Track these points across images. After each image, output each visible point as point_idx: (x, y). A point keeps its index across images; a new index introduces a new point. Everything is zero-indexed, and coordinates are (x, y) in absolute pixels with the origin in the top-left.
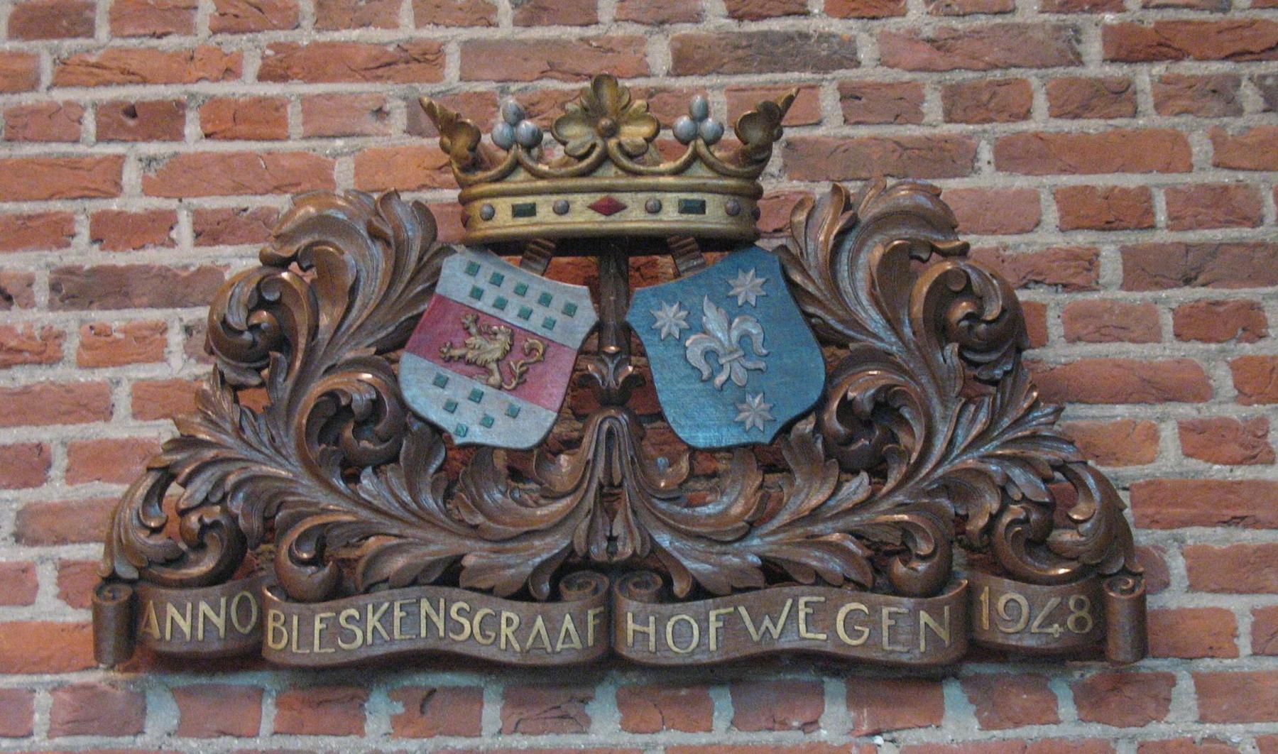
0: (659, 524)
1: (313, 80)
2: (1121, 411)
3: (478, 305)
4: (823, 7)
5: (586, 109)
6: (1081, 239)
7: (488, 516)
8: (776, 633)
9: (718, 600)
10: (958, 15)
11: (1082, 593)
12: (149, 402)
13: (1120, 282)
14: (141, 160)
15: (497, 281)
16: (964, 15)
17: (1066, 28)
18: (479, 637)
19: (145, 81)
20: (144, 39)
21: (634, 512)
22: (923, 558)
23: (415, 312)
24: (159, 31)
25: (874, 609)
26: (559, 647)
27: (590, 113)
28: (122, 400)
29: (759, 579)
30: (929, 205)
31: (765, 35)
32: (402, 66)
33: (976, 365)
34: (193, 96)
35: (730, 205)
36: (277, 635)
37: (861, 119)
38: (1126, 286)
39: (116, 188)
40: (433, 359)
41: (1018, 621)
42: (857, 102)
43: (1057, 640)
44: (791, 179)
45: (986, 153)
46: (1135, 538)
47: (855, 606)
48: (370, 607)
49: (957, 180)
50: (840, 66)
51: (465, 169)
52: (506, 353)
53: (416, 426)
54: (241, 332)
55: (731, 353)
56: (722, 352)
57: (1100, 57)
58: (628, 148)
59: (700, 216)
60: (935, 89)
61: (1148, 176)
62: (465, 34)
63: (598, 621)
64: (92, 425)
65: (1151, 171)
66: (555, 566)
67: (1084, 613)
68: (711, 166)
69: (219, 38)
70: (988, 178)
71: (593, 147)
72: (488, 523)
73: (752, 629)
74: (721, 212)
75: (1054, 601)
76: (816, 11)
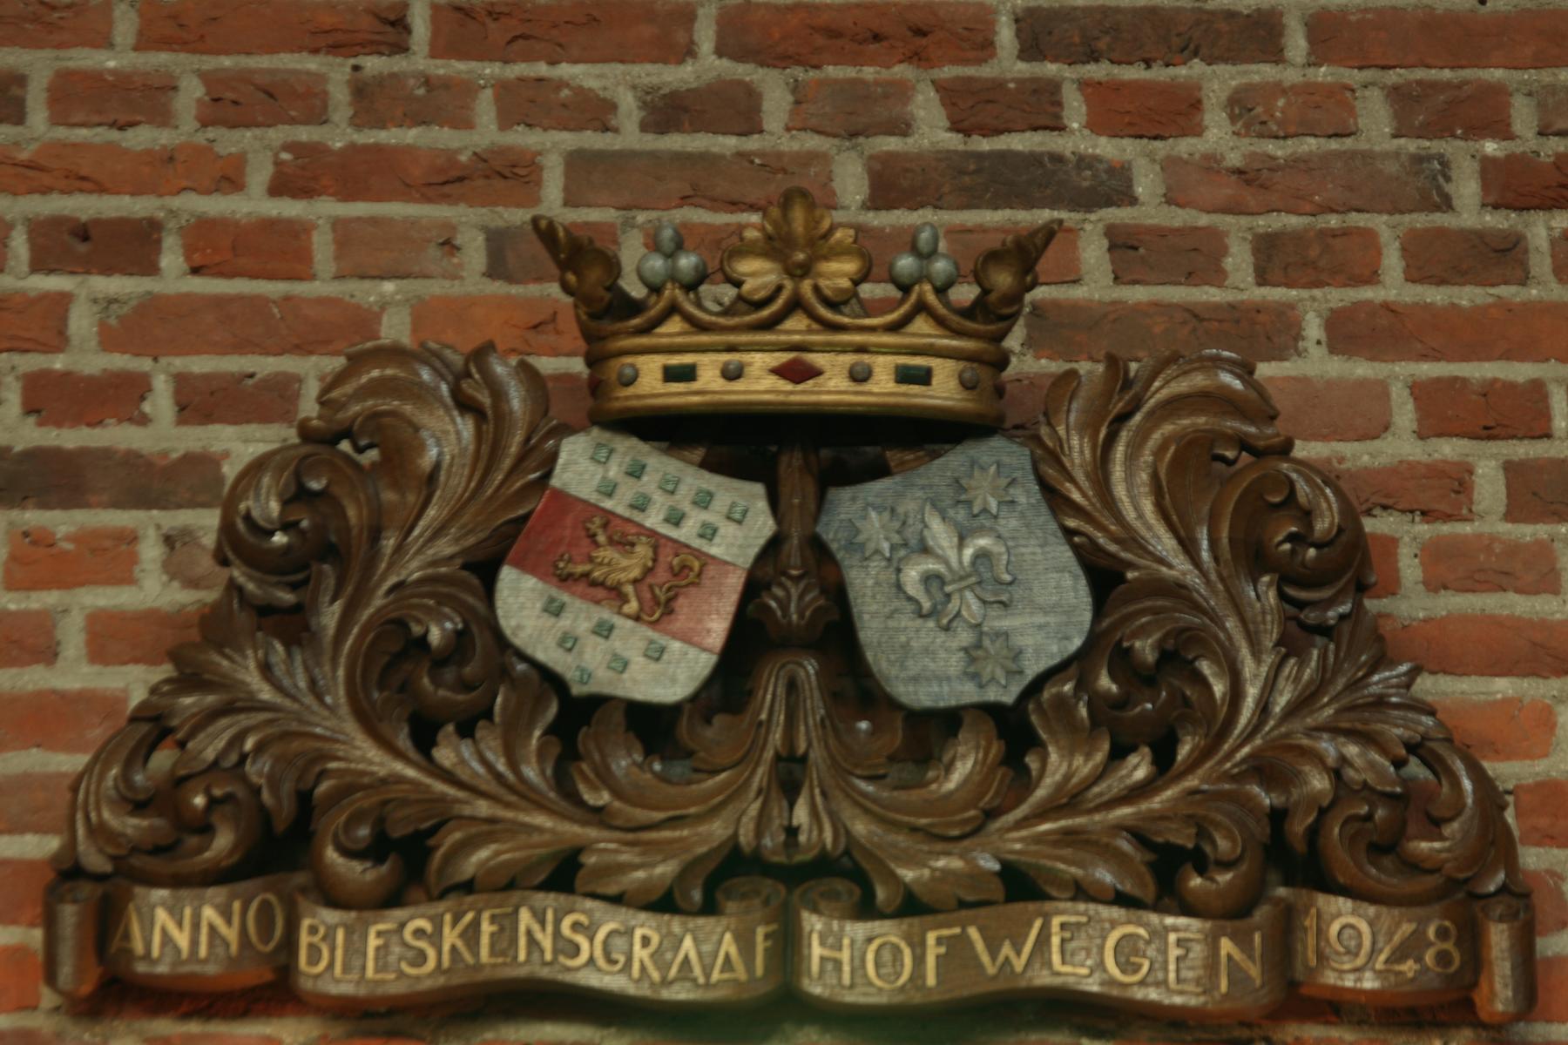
0: (857, 811)
1: (348, 196)
2: (1503, 686)
3: (608, 504)
4: (1084, 119)
5: (769, 238)
6: (1448, 449)
7: (617, 793)
8: (1019, 964)
9: (941, 917)
10: (1277, 137)
11: (1446, 917)
12: (109, 637)
13: (1502, 509)
14: (95, 301)
15: (636, 472)
16: (1285, 138)
17: (1429, 158)
18: (601, 962)
19: (101, 189)
20: (99, 130)
21: (824, 794)
22: (1226, 865)
23: (521, 512)
24: (123, 118)
25: (1160, 934)
26: (716, 976)
27: (776, 246)
28: (73, 639)
29: (997, 890)
30: (1237, 384)
31: (1003, 156)
32: (480, 182)
33: (1301, 605)
34: (172, 213)
35: (967, 375)
36: (314, 951)
37: (1135, 277)
38: (1510, 516)
39: (59, 341)
40: (542, 577)
41: (1357, 955)
42: (1131, 253)
43: (1413, 980)
44: (1038, 358)
45: (1313, 329)
46: (1521, 861)
47: (1130, 929)
48: (448, 918)
49: (1273, 364)
50: (1109, 203)
51: (593, 316)
52: (648, 571)
53: (521, 667)
54: (272, 533)
55: (962, 578)
56: (948, 577)
57: (1477, 200)
58: (828, 292)
59: (923, 388)
60: (1244, 239)
61: (1544, 366)
62: (569, 140)
63: (769, 943)
64: (28, 669)
65: (1547, 360)
66: (711, 866)
67: (1449, 946)
68: (940, 321)
69: (211, 133)
70: (1316, 362)
71: (779, 289)
72: (617, 804)
73: (985, 958)
74: (953, 384)
75: (1407, 928)
76: (1075, 125)
